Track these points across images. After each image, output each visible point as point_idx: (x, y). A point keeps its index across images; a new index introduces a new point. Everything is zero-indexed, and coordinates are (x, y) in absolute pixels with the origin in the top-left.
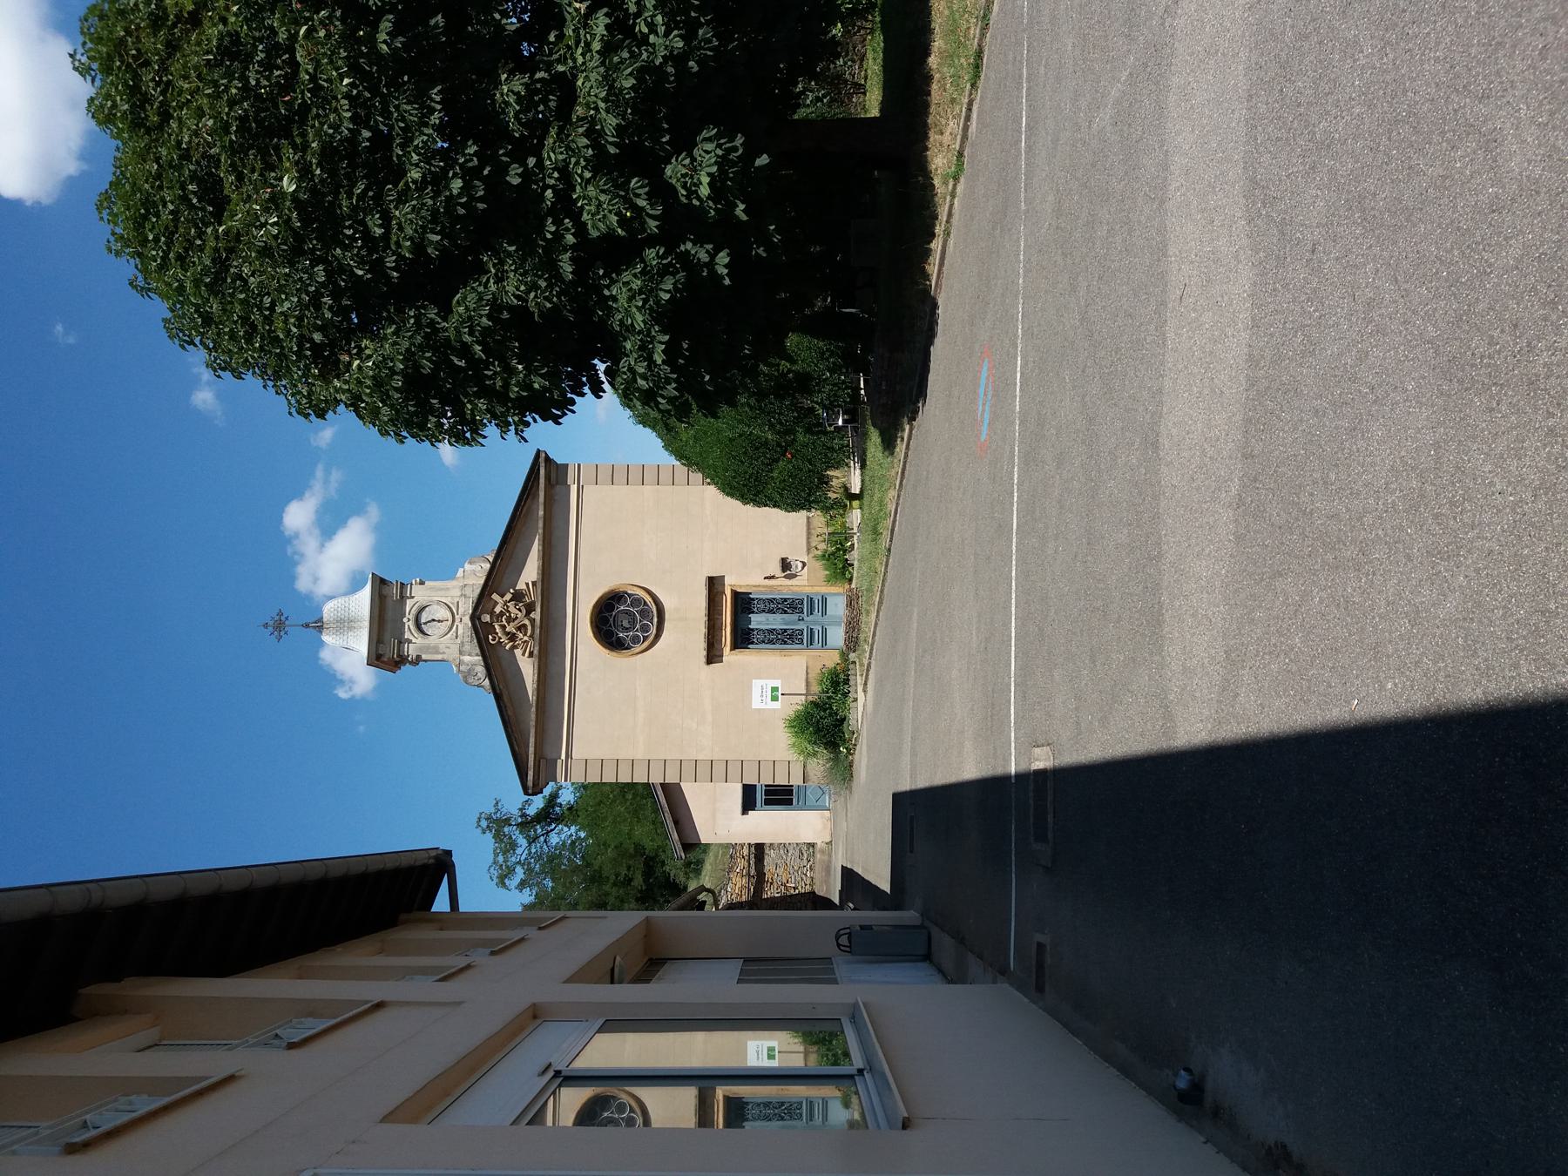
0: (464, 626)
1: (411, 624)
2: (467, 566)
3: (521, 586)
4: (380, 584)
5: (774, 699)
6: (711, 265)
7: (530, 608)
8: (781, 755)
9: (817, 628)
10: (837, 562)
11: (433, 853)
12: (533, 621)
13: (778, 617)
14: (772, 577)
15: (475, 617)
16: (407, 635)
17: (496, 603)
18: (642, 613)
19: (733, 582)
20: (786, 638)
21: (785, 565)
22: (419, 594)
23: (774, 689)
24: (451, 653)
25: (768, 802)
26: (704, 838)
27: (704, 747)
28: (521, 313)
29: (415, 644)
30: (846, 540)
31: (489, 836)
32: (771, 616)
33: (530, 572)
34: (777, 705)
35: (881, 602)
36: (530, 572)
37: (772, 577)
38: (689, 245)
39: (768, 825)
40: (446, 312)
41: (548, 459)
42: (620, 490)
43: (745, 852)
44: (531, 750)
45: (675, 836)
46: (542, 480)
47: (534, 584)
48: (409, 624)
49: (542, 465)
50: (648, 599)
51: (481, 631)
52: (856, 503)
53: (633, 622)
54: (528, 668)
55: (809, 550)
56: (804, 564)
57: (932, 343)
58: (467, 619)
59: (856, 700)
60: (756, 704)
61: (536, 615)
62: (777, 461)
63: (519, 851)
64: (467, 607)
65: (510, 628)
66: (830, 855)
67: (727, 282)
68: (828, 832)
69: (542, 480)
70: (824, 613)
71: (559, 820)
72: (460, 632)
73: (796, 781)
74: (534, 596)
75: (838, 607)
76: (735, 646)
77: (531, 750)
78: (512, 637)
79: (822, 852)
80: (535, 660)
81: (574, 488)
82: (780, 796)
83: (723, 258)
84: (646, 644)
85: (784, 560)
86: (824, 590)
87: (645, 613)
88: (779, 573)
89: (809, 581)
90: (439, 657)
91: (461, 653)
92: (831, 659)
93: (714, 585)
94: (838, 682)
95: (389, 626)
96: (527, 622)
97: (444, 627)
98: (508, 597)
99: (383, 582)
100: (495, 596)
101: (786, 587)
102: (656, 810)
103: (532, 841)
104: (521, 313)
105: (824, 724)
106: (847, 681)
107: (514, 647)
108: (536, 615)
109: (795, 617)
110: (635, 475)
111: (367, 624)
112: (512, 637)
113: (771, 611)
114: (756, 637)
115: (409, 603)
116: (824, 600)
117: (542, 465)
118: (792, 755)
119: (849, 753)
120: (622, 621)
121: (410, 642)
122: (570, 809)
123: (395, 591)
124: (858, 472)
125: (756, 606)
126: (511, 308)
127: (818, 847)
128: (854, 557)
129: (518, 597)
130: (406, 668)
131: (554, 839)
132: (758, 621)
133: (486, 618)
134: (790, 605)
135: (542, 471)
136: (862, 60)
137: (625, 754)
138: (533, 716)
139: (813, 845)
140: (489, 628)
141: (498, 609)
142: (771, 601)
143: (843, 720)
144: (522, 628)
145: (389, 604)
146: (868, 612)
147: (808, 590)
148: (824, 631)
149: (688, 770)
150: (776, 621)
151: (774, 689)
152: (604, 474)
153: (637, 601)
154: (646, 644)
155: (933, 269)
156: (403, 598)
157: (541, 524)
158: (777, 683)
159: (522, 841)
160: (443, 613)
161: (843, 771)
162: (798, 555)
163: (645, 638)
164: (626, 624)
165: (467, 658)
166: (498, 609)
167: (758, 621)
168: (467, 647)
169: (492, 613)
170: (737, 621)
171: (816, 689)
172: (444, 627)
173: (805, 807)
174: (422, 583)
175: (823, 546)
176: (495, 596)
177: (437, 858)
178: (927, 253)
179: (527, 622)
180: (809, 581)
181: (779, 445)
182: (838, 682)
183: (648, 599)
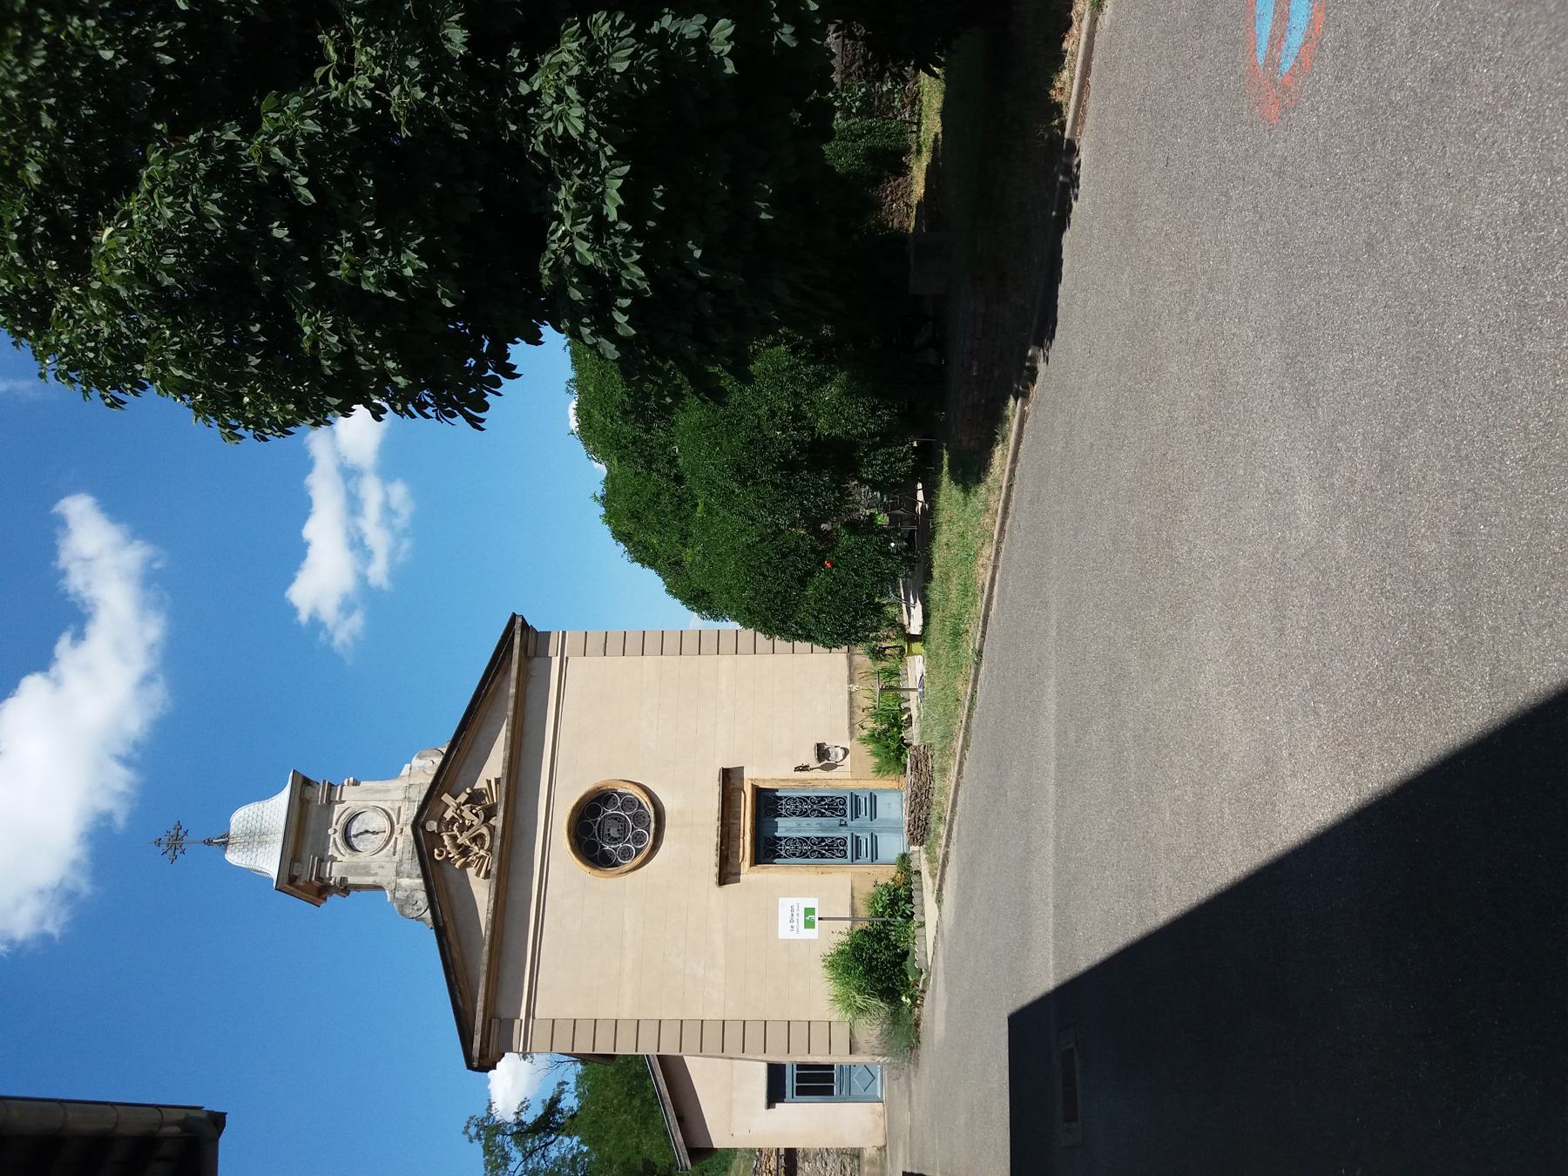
0: (404, 840)
1: (338, 837)
2: (416, 762)
3: (481, 784)
4: (303, 784)
5: (809, 924)
6: (703, 41)
7: (490, 812)
8: (817, 1010)
9: (865, 836)
10: (890, 741)
11: (180, 1115)
12: (492, 829)
13: (814, 821)
14: (804, 768)
15: (418, 825)
16: (332, 851)
17: (447, 806)
18: (635, 818)
19: (757, 774)
20: (822, 850)
21: (822, 752)
22: (351, 798)
23: (809, 911)
24: (385, 876)
25: (801, 1092)
26: (719, 1140)
27: (713, 1002)
28: (376, 124)
29: (341, 863)
30: (903, 711)
31: (478, 1147)
32: (804, 821)
33: (494, 767)
34: (812, 934)
35: (965, 746)
36: (494, 767)
37: (804, 768)
38: (667, 21)
39: (803, 1123)
40: (251, 127)
41: (524, 624)
42: (614, 663)
43: (773, 1164)
44: (480, 1005)
45: (679, 1138)
46: (516, 651)
47: (497, 781)
48: (335, 836)
49: (518, 632)
50: (644, 799)
51: (425, 842)
52: (916, 646)
53: (624, 830)
54: (482, 892)
55: (852, 734)
56: (846, 752)
57: (1063, 222)
58: (408, 830)
59: (922, 925)
60: (784, 932)
61: (498, 821)
62: (810, 574)
63: (512, 1167)
64: (409, 812)
65: (463, 839)
66: (883, 1166)
67: (730, 68)
68: (880, 1132)
69: (516, 651)
70: (873, 815)
71: (559, 1129)
72: (399, 846)
73: (839, 1057)
74: (497, 797)
75: (894, 806)
76: (757, 860)
77: (480, 1005)
78: (464, 851)
79: (872, 1162)
80: (492, 881)
81: (556, 661)
82: (817, 1082)
83: (724, 28)
84: (639, 859)
85: (820, 747)
86: (875, 784)
87: (639, 819)
88: (813, 763)
89: (854, 772)
90: (369, 880)
91: (398, 874)
92: (886, 874)
93: (730, 779)
94: (898, 902)
95: (309, 840)
96: (484, 831)
97: (379, 840)
98: (463, 798)
99: (307, 782)
100: (446, 798)
101: (824, 782)
102: (653, 1102)
103: (528, 1155)
104: (376, 124)
105: (879, 964)
106: (909, 899)
107: (466, 865)
108: (498, 821)
109: (835, 821)
110: (633, 643)
111: (281, 836)
112: (464, 851)
113: (804, 814)
114: (784, 848)
115: (338, 809)
116: (873, 799)
117: (518, 632)
118: (837, 1014)
119: (914, 1003)
120: (610, 829)
121: (333, 859)
122: (572, 1117)
123: (320, 794)
124: (919, 605)
125: (785, 807)
126: (361, 115)
127: (866, 1155)
128: (913, 735)
129: (475, 798)
130: (334, 899)
131: (553, 1153)
132: (786, 827)
133: (432, 826)
134: (828, 806)
135: (517, 640)
136: (913, 104)
137: (606, 1012)
138: (485, 958)
139: (856, 1154)
140: (436, 838)
141: (448, 815)
142: (803, 800)
143: (905, 954)
144: (477, 839)
145: (313, 811)
146: (944, 771)
147: (852, 785)
148: (874, 839)
149: (691, 1041)
150: (811, 827)
151: (809, 911)
152: (595, 642)
153: (630, 803)
154: (639, 859)
155: (1067, 83)
156: (330, 803)
157: (511, 705)
158: (812, 902)
159: (516, 1155)
160: (380, 822)
161: (905, 1034)
162: (838, 739)
163: (638, 851)
164: (614, 833)
165: (405, 882)
166: (448, 815)
167: (786, 827)
168: (406, 867)
169: (441, 820)
170: (760, 828)
171: (864, 912)
172: (379, 840)
173: (850, 1098)
174: (356, 783)
175: (870, 724)
176: (446, 798)
177: (186, 1124)
178: (1057, 60)
179: (484, 831)
180: (854, 772)
181: (813, 550)
182: (898, 902)
183: (644, 799)
